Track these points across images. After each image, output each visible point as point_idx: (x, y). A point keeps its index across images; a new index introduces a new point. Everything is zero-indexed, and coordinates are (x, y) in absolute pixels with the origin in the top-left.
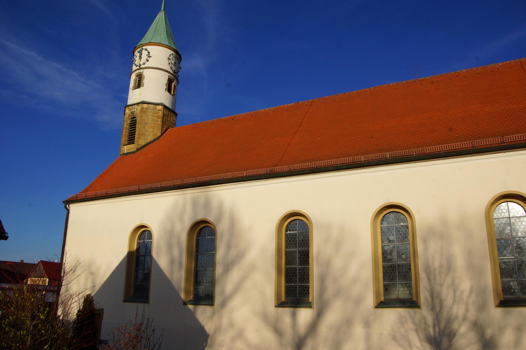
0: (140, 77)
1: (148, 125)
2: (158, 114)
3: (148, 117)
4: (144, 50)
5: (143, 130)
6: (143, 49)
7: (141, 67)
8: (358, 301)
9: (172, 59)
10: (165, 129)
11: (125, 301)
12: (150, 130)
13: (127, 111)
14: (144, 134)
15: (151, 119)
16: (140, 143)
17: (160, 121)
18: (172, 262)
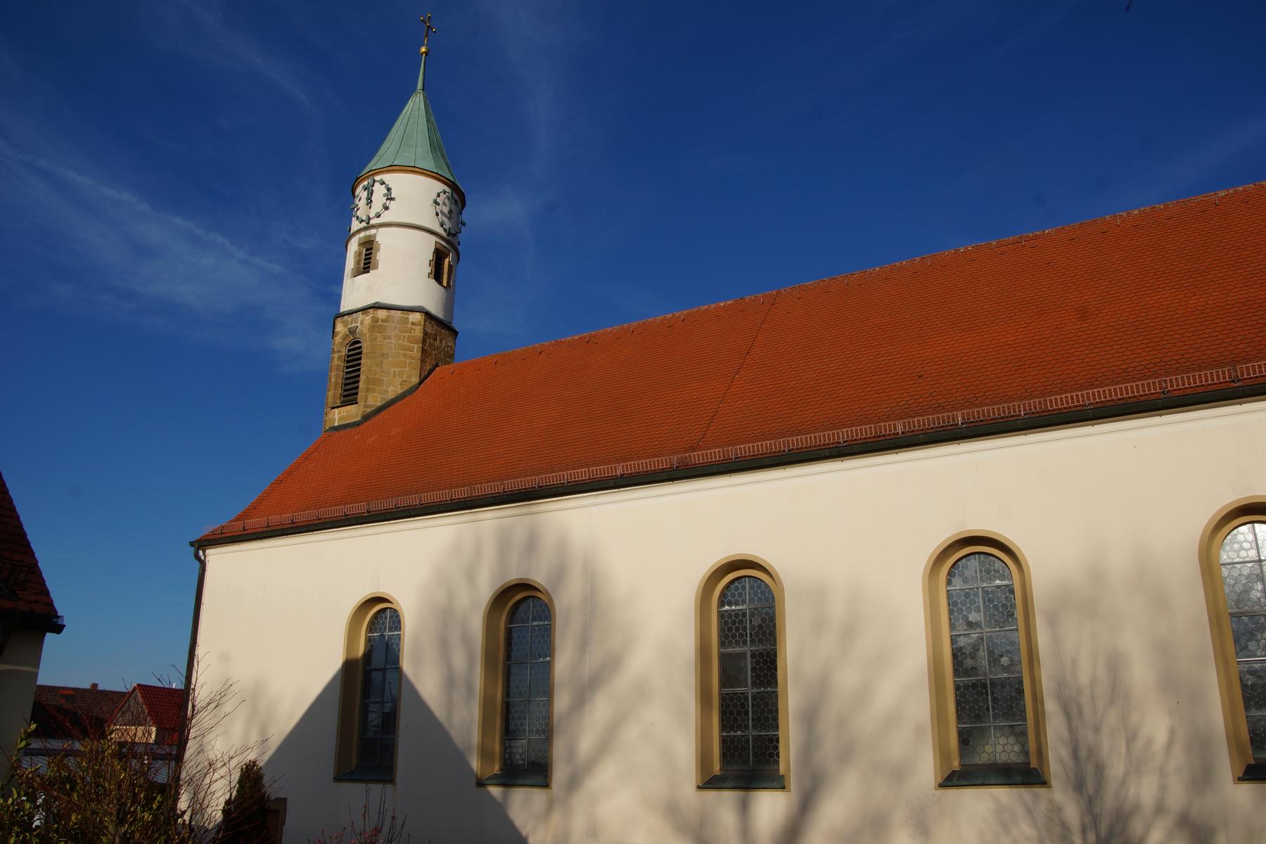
0: (369, 248)
1: (390, 359)
2: (413, 331)
4: (377, 185)
5: (378, 370)
6: (374, 181)
7: (372, 222)
8: (899, 774)
12: (394, 372)
13: (340, 328)
15: (395, 344)
16: (370, 402)
18: (450, 682)
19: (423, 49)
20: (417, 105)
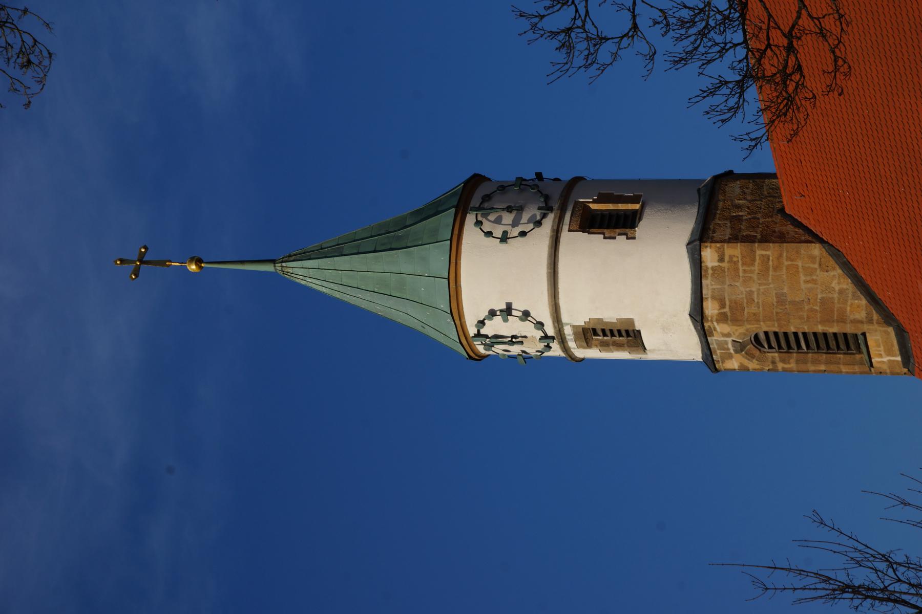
0: (588, 334)
1: (785, 290)
2: (735, 259)
3: (756, 293)
4: (483, 332)
5: (806, 308)
6: (478, 335)
7: (550, 331)
9: (498, 221)
10: (790, 228)
12: (807, 282)
14: (823, 302)
15: (760, 284)
16: (862, 315)
17: (763, 250)
19: (193, 267)
20: (312, 272)
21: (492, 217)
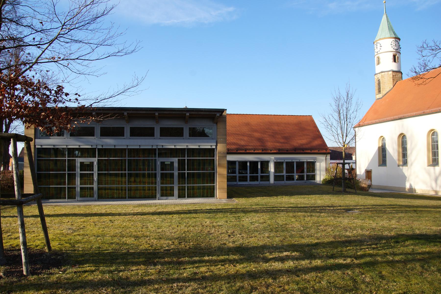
0: (378, 58)
9: (394, 43)
10: (395, 83)
11: (379, 166)
16: (383, 93)
18: (394, 149)
21: (394, 42)
